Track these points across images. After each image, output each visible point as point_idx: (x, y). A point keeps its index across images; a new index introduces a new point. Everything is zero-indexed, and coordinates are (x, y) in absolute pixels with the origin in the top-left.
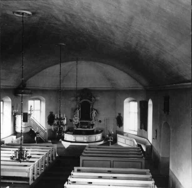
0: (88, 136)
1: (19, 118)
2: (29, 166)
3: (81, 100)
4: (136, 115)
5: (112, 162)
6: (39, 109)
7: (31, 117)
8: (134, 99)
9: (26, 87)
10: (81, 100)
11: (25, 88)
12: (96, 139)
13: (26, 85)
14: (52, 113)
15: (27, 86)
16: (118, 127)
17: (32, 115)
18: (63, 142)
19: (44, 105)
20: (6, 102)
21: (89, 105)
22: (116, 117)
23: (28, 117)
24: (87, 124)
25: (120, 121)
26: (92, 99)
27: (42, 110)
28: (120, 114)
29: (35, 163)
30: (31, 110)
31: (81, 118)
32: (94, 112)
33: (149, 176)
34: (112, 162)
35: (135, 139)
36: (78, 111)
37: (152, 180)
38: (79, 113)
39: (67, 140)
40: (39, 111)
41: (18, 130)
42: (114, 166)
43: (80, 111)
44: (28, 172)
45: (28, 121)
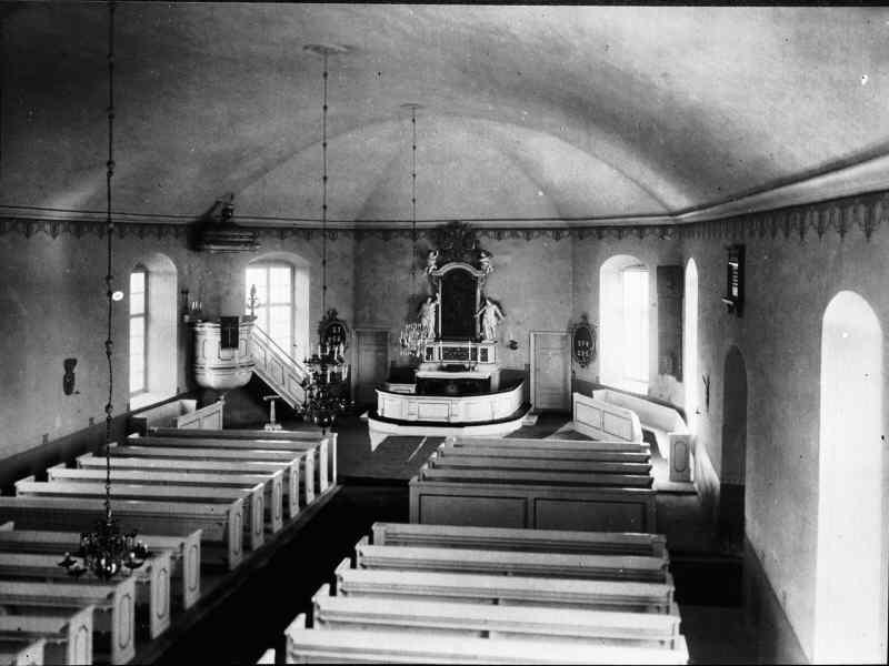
0: (297, 502)
1: (210, 336)
2: (230, 501)
3: (439, 265)
4: (646, 322)
5: (531, 505)
6: (289, 301)
7: (254, 330)
8: (638, 261)
9: (229, 217)
10: (439, 265)
11: (230, 220)
12: (493, 414)
13: (232, 211)
14: (335, 313)
15: (235, 214)
16: (577, 366)
17: (255, 322)
18: (373, 424)
19: (303, 281)
20: (158, 274)
21: (471, 283)
22: (504, 367)
23: (240, 329)
24: (462, 354)
25: (582, 339)
26: (481, 264)
27: (297, 303)
28: (585, 317)
29: (255, 489)
30: (253, 303)
31: (443, 333)
32: (491, 310)
33: (662, 591)
34: (531, 505)
35: (637, 413)
36: (433, 305)
37: (668, 612)
38: (437, 312)
39: (386, 415)
40: (289, 309)
41: (210, 378)
42: (538, 525)
43: (437, 307)
44: (224, 522)
45: (242, 344)
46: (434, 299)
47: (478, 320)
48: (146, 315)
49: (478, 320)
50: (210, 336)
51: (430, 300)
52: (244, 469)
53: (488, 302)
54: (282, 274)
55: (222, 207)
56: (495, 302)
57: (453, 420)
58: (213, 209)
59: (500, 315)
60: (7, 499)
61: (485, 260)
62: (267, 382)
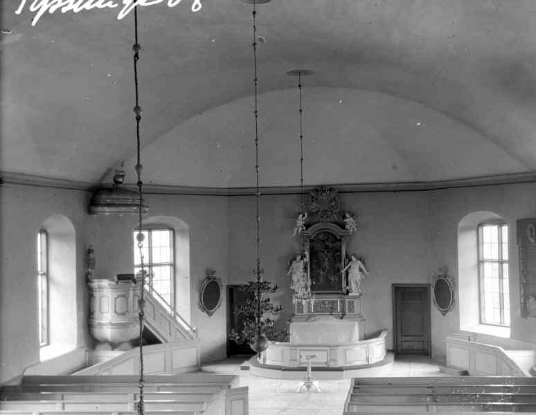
19: (184, 246)
36: (301, 264)
46: (303, 257)
47: (344, 276)
48: (47, 275)
49: (344, 276)
50: (106, 293)
51: (299, 257)
52: (187, 406)
53: (353, 258)
54: (161, 238)
55: (113, 174)
56: (360, 259)
57: (332, 365)
58: (106, 174)
59: (364, 269)
60: (524, 213)
61: (349, 220)
62: (153, 332)
